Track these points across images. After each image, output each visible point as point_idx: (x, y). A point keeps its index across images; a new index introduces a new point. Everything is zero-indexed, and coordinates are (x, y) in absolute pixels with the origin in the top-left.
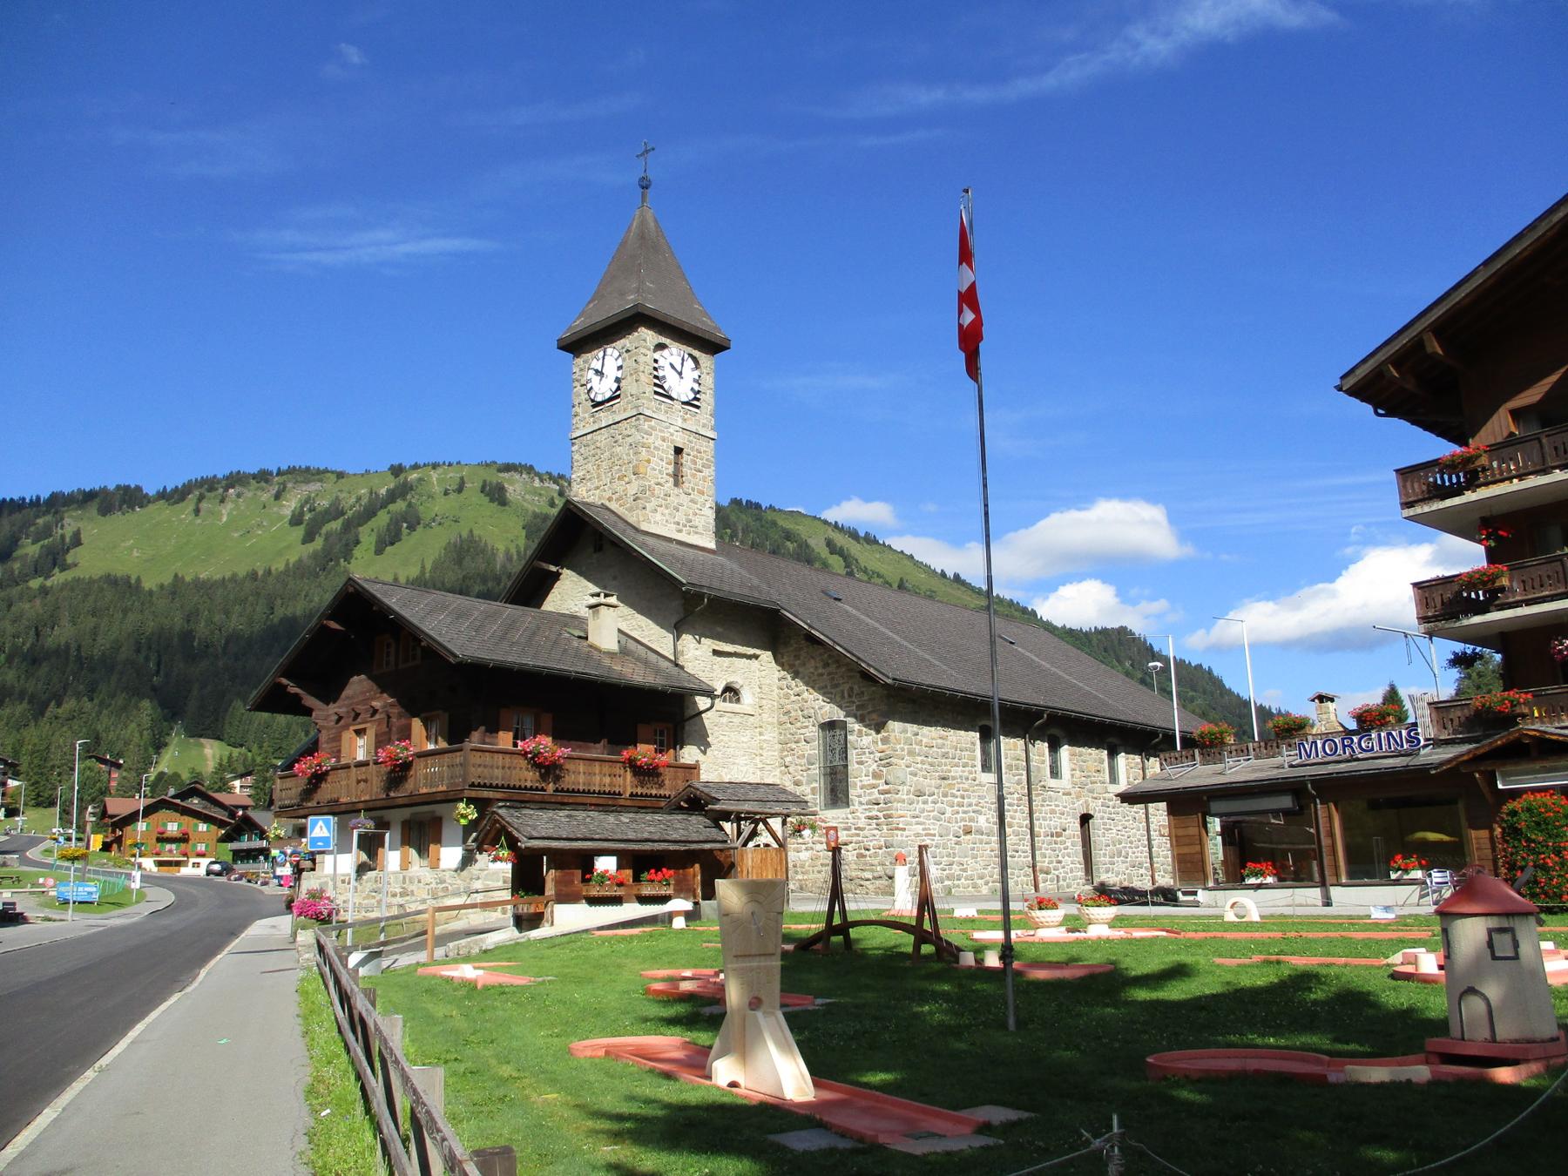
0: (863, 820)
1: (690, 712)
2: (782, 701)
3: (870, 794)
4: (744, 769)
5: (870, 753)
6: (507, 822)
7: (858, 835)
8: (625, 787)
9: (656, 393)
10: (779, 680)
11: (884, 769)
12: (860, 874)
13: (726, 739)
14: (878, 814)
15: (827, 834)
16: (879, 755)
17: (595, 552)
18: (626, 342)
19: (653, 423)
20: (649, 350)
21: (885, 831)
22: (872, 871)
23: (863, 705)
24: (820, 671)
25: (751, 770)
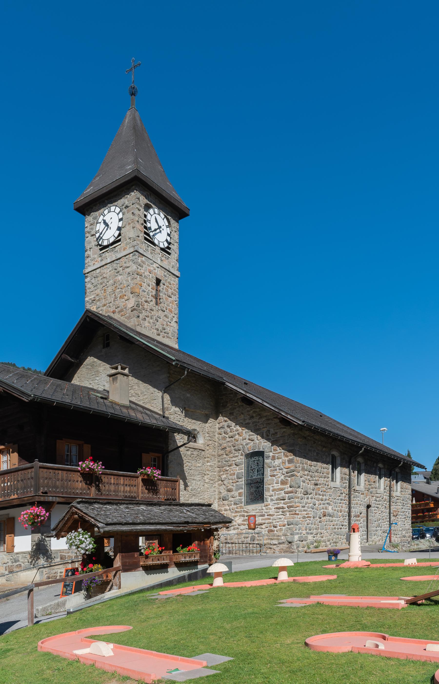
0: (273, 510)
1: (171, 447)
2: (221, 442)
3: (278, 494)
4: (199, 483)
5: (280, 469)
6: (84, 513)
7: (269, 519)
8: (138, 492)
9: (146, 239)
10: (219, 429)
11: (289, 479)
12: (269, 541)
13: (190, 464)
14: (284, 506)
15: (249, 519)
16: (286, 470)
17: (104, 348)
18: (125, 201)
19: (144, 258)
20: (141, 206)
21: (288, 515)
22: (278, 539)
23: (276, 440)
24: (247, 421)
25: (202, 484)
